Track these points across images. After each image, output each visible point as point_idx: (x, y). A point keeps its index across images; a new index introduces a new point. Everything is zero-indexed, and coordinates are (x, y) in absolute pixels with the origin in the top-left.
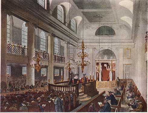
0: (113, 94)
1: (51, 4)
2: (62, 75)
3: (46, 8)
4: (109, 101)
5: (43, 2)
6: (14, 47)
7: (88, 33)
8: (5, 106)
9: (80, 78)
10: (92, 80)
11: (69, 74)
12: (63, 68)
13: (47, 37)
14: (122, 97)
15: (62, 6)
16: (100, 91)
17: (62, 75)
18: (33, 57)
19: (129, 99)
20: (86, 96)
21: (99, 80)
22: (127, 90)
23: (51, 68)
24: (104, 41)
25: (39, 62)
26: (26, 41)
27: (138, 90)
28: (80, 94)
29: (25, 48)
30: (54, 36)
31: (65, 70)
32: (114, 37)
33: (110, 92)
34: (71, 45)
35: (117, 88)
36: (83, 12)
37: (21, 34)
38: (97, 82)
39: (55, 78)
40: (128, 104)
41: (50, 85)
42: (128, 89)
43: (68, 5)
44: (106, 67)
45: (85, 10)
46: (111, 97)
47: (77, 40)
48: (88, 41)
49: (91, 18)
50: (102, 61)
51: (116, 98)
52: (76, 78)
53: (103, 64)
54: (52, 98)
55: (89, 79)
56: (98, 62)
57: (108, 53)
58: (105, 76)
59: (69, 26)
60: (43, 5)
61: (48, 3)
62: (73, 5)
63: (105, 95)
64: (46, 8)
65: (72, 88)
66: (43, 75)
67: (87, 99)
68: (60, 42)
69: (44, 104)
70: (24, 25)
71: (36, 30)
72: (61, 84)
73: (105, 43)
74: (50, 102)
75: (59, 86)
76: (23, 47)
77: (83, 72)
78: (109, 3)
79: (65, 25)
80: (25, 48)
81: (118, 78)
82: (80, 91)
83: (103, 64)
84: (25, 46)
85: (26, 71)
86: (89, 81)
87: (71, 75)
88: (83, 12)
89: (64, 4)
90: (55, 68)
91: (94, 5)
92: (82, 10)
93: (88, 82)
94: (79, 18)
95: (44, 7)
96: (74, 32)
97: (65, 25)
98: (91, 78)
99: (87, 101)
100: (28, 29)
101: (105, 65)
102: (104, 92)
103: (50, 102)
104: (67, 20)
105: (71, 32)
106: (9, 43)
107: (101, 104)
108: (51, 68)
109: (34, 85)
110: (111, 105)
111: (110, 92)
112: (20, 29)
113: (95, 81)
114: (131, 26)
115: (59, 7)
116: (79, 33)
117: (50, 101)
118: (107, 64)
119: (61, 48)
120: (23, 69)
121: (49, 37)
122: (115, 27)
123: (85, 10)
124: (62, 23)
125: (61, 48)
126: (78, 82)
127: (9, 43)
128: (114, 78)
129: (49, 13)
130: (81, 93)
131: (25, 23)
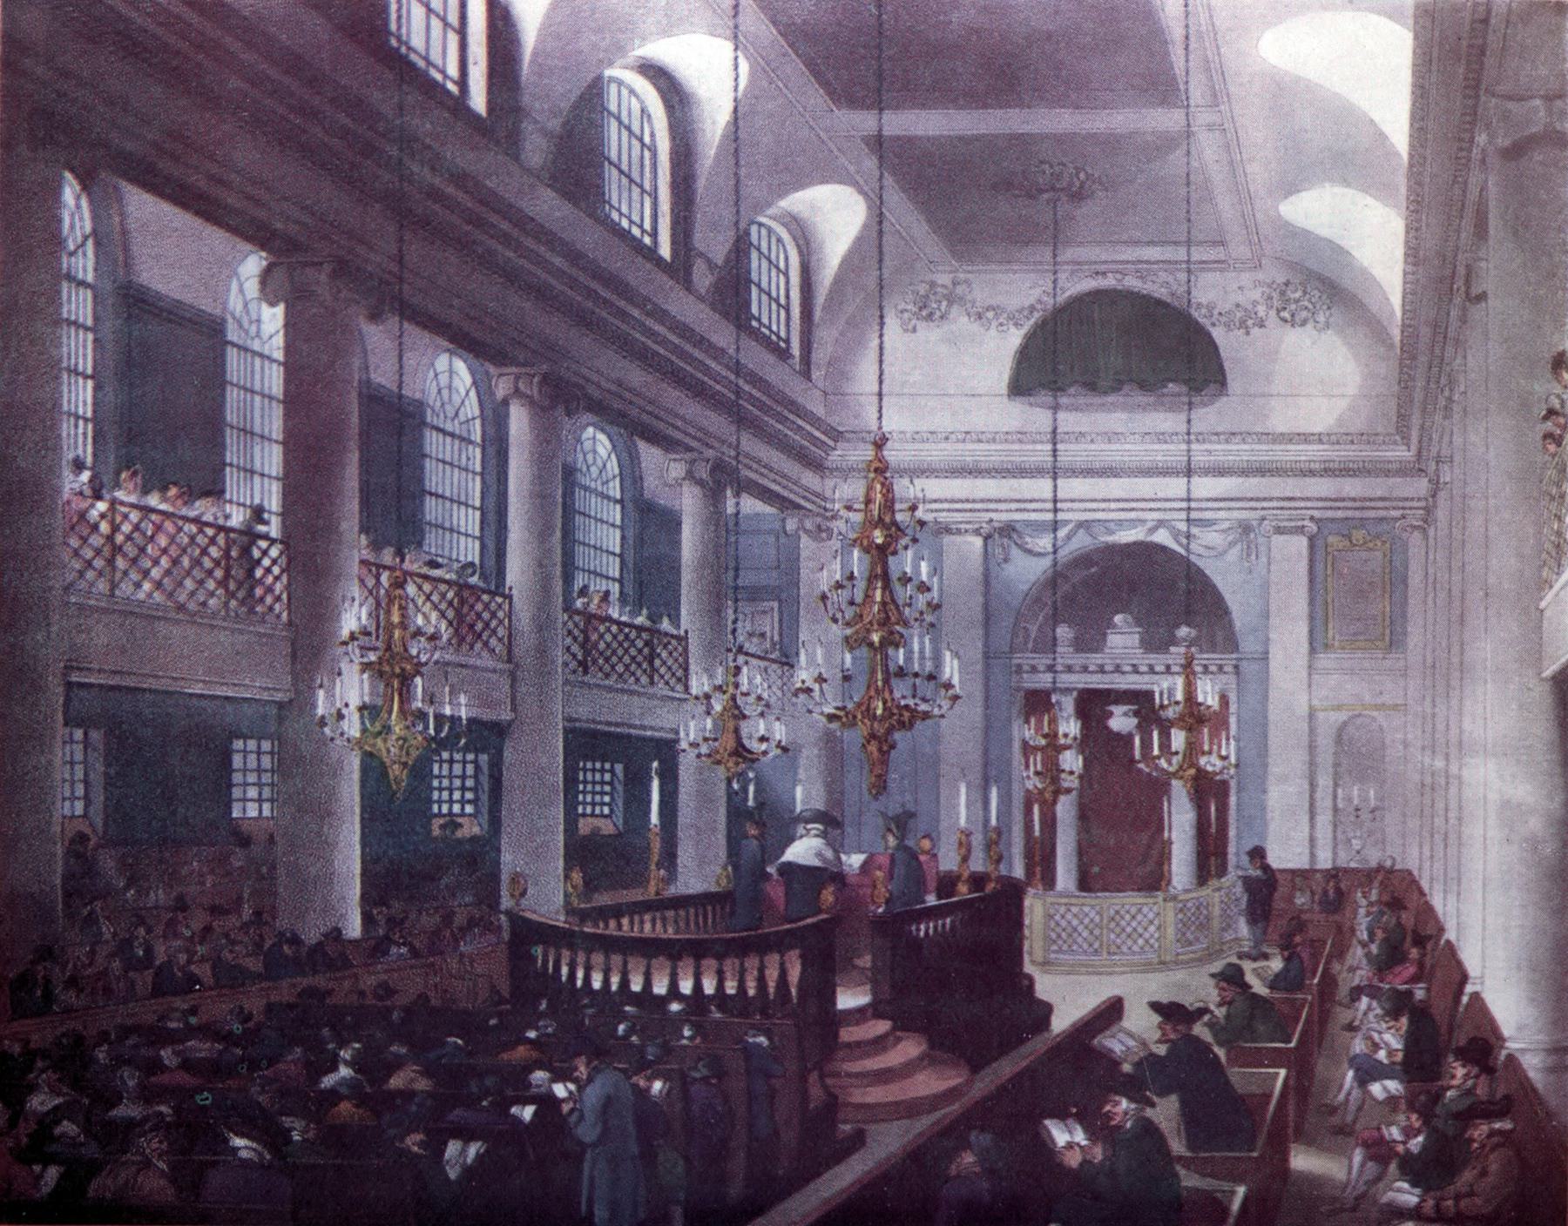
0: (1200, 1030)
1: (535, 54)
2: (654, 818)
3: (478, 100)
4: (1166, 1112)
5: (453, 40)
6: (134, 516)
7: (940, 393)
8: (47, 1161)
9: (855, 860)
10: (978, 881)
11: (737, 813)
12: (666, 750)
13: (495, 419)
14: (1301, 1064)
15: (658, 74)
16: (1068, 1000)
17: (654, 818)
18: (345, 633)
19: (1376, 1089)
20: (910, 1048)
21: (1049, 881)
22: (1356, 993)
23: (539, 756)
24: (1115, 453)
25: (406, 680)
26: (272, 459)
27: (1469, 989)
28: (848, 1034)
29: (262, 528)
30: (562, 397)
31: (687, 765)
32: (1208, 417)
33: (1170, 1012)
34: (751, 505)
35: (1247, 966)
36: (878, 143)
37: (216, 380)
38: (1035, 907)
39: (581, 851)
40: (1366, 1145)
41: (527, 933)
42: (1362, 975)
43: (712, 68)
44: (1127, 740)
45: (906, 122)
46: (1185, 1064)
47: (815, 441)
48: (936, 453)
49: (967, 201)
50: (1085, 669)
51: (1240, 1077)
52: (804, 849)
53: (1092, 705)
54: (554, 1080)
55: (948, 861)
56: (1044, 681)
57: (1156, 587)
58: (1121, 853)
59: (733, 291)
60: (453, 70)
61: (502, 25)
62: (764, 70)
63: (1114, 1043)
64: (478, 100)
65: (761, 970)
66: (452, 823)
67: (927, 1084)
68: (631, 474)
69: (467, 1135)
70: (252, 288)
71: (378, 338)
72: (648, 928)
73: (1129, 472)
74: (528, 1113)
75: (610, 945)
76: (237, 518)
77: (880, 787)
78: (1153, 37)
79: (688, 285)
80: (262, 528)
81: (1258, 854)
82: (848, 1000)
83: (1092, 705)
84: (258, 513)
85: (266, 778)
86: (947, 884)
87: (756, 822)
88: (878, 143)
89: (661, 50)
90: (587, 744)
91: (1003, 72)
92: (866, 121)
93: (932, 900)
94: (836, 214)
95: (655, 242)
96: (783, 354)
97: (688, 285)
98: (965, 859)
99: (911, 1109)
100: (290, 325)
101: (1121, 720)
102: (1112, 1011)
103: (528, 1113)
104: (714, 244)
105: (755, 357)
106: (85, 476)
107: (1080, 1137)
108: (539, 756)
109: (354, 927)
110: (1177, 1146)
111: (1170, 1012)
112: (210, 332)
113: (1013, 893)
114: (1396, 300)
115: (620, 83)
116: (840, 370)
117: (525, 1102)
118: (1141, 701)
119: (650, 521)
120: (237, 761)
121: (519, 421)
122: (1214, 295)
123: (906, 122)
124: (659, 261)
125: (650, 521)
126: (828, 896)
127: (85, 476)
128: (1210, 853)
129: (512, 144)
130: (859, 1015)
131: (252, 265)
